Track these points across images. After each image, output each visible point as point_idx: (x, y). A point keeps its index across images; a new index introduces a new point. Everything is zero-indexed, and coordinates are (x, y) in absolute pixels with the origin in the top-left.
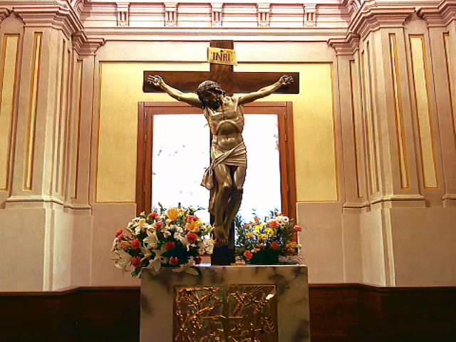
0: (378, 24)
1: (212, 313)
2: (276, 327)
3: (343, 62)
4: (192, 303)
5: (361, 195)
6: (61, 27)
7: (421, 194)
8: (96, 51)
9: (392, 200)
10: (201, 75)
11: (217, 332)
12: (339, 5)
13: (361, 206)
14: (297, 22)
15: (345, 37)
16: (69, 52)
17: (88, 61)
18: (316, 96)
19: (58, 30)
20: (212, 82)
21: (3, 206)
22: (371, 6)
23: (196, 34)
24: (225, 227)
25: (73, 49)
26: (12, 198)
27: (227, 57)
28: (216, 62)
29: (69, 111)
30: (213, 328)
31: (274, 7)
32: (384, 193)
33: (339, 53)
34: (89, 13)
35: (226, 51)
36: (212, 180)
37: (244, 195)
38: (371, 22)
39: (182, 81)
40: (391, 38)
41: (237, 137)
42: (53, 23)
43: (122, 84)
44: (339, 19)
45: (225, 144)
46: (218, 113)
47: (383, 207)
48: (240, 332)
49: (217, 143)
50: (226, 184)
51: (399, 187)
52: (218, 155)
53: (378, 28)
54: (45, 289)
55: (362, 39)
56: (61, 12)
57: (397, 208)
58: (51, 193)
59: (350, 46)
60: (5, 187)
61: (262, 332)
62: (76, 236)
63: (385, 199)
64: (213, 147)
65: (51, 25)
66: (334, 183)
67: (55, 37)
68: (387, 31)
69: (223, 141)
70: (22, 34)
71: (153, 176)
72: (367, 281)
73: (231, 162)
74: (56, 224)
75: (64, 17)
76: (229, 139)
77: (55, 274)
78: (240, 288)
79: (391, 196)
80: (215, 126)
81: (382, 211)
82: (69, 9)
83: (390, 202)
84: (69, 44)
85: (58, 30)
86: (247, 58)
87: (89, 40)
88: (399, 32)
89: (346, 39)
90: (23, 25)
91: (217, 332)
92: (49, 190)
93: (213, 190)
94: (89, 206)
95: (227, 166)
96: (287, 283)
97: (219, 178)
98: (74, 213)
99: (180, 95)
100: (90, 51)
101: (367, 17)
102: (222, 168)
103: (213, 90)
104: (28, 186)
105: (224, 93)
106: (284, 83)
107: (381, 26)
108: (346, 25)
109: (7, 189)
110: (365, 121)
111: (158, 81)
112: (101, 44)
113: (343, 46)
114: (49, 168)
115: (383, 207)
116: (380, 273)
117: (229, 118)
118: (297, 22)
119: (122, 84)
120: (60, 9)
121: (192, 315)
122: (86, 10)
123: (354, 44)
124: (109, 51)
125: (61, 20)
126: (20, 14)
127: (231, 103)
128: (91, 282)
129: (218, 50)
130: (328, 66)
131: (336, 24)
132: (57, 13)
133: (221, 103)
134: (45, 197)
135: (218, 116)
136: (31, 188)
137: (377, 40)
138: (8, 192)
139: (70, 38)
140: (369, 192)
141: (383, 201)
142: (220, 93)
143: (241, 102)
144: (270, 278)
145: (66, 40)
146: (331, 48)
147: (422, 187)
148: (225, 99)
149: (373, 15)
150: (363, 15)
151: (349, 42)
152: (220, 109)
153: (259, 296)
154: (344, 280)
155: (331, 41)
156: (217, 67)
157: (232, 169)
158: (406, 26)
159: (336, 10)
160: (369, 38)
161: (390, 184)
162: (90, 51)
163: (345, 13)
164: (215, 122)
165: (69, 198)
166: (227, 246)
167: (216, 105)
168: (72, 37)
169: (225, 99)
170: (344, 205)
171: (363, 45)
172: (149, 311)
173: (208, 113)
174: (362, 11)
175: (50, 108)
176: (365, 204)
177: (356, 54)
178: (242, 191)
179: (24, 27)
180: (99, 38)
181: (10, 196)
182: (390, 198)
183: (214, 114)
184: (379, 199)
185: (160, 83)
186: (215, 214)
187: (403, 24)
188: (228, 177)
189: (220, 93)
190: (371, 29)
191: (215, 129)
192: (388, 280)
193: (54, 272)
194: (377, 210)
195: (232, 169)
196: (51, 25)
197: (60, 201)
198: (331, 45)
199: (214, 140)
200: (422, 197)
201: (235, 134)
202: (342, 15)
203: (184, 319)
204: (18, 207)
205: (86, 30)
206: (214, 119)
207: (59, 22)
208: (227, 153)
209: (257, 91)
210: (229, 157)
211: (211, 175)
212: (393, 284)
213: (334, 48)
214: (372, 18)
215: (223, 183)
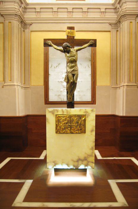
0: (126, 18)
1: (67, 123)
2: (85, 128)
3: (114, 31)
4: (61, 120)
5: (117, 83)
6: (17, 20)
7: (136, 83)
8: (29, 27)
9: (127, 85)
10: (64, 40)
11: (68, 129)
12: (114, 8)
13: (116, 87)
14: (97, 15)
15: (115, 21)
16: (20, 28)
17: (27, 31)
18: (104, 43)
19: (16, 21)
20: (67, 43)
21: (3, 87)
22: (124, 11)
23: (64, 20)
24: (71, 95)
25: (22, 27)
26: (5, 84)
27: (73, 33)
28: (69, 35)
29: (21, 51)
30: (67, 128)
31: (89, 9)
32: (124, 83)
33: (113, 27)
34: (26, 12)
35: (72, 31)
36: (67, 79)
37: (77, 85)
38: (124, 17)
39: (58, 42)
40: (131, 24)
41: (75, 63)
42: (14, 18)
43: (37, 40)
44: (114, 14)
45: (71, 66)
46: (69, 55)
47: (124, 88)
48: (75, 129)
49: (69, 66)
50: (71, 81)
51: (129, 81)
52: (69, 70)
53: (126, 20)
54: (17, 115)
55: (121, 23)
56: (17, 14)
57: (128, 88)
58: (17, 82)
59: (117, 25)
60: (3, 80)
61: (81, 129)
62: (26, 97)
63: (124, 85)
64: (68, 67)
65: (13, 19)
66: (109, 78)
67: (16, 23)
68: (129, 21)
69: (71, 65)
70: (4, 23)
71: (49, 75)
72: (117, 114)
73: (74, 73)
74: (19, 94)
75: (18, 16)
76: (73, 64)
77: (20, 112)
78: (75, 116)
79: (126, 84)
80: (68, 59)
81: (123, 89)
82: (20, 13)
83: (126, 86)
84: (20, 25)
85: (16, 21)
86: (78, 36)
87: (27, 23)
88: (133, 21)
89: (115, 22)
90: (4, 19)
91: (68, 129)
92: (17, 81)
93: (68, 82)
94: (29, 87)
95: (72, 74)
96: (89, 114)
97: (69, 78)
98: (25, 89)
99: (57, 48)
100: (27, 27)
101: (123, 15)
102: (70, 75)
103: (67, 46)
104: (10, 80)
105: (71, 47)
106: (91, 43)
107: (128, 19)
108: (116, 17)
109: (3, 81)
110: (120, 55)
111: (50, 42)
112: (31, 24)
113: (115, 25)
114: (16, 73)
115: (124, 88)
116: (121, 112)
117: (73, 57)
118: (97, 15)
119: (37, 40)
120: (17, 13)
121: (61, 124)
122: (25, 11)
123: (118, 24)
124: (34, 27)
125: (17, 17)
126: (3, 15)
127: (73, 51)
128: (31, 113)
129: (69, 30)
130: (108, 33)
131: (112, 16)
132: (16, 14)
133: (70, 51)
134: (15, 84)
135: (69, 56)
136: (11, 81)
137: (125, 24)
138: (4, 82)
139: (20, 23)
140: (120, 82)
141: (124, 86)
142: (70, 47)
143: (77, 51)
144: (84, 113)
145: (19, 24)
146: (110, 25)
147: (136, 81)
148: (71, 49)
149: (125, 15)
150: (121, 15)
151: (117, 23)
152: (70, 53)
153: (80, 118)
154: (110, 113)
155: (110, 23)
156: (69, 37)
157: (73, 75)
158: (137, 19)
159: (113, 11)
160: (123, 23)
161: (126, 80)
162: (27, 27)
163: (116, 11)
164: (68, 58)
165: (22, 83)
166: (72, 102)
167: (68, 52)
168: (21, 22)
169: (72, 50)
170: (112, 87)
171: (121, 25)
172: (49, 123)
173: (66, 55)
174: (121, 13)
175: (15, 49)
176: (118, 86)
177: (119, 28)
178: (76, 83)
179: (5, 20)
180: (30, 22)
181: (5, 83)
182: (126, 85)
183: (68, 55)
184: (122, 85)
185: (51, 43)
186: (68, 91)
187: (136, 18)
188: (72, 78)
189: (70, 47)
190: (124, 20)
191: (68, 60)
192: (123, 113)
193: (20, 108)
194: (122, 88)
195: (73, 75)
196: (13, 19)
197: (20, 85)
198: (110, 24)
199: (68, 65)
200: (136, 85)
201: (74, 63)
202: (115, 12)
203: (58, 125)
204: (7, 87)
205: (25, 19)
206: (68, 57)
207: (17, 18)
208: (72, 69)
209: (82, 46)
210: (73, 71)
211: (67, 77)
212: (124, 115)
213: (111, 25)
214: (124, 16)
215: (70, 81)
